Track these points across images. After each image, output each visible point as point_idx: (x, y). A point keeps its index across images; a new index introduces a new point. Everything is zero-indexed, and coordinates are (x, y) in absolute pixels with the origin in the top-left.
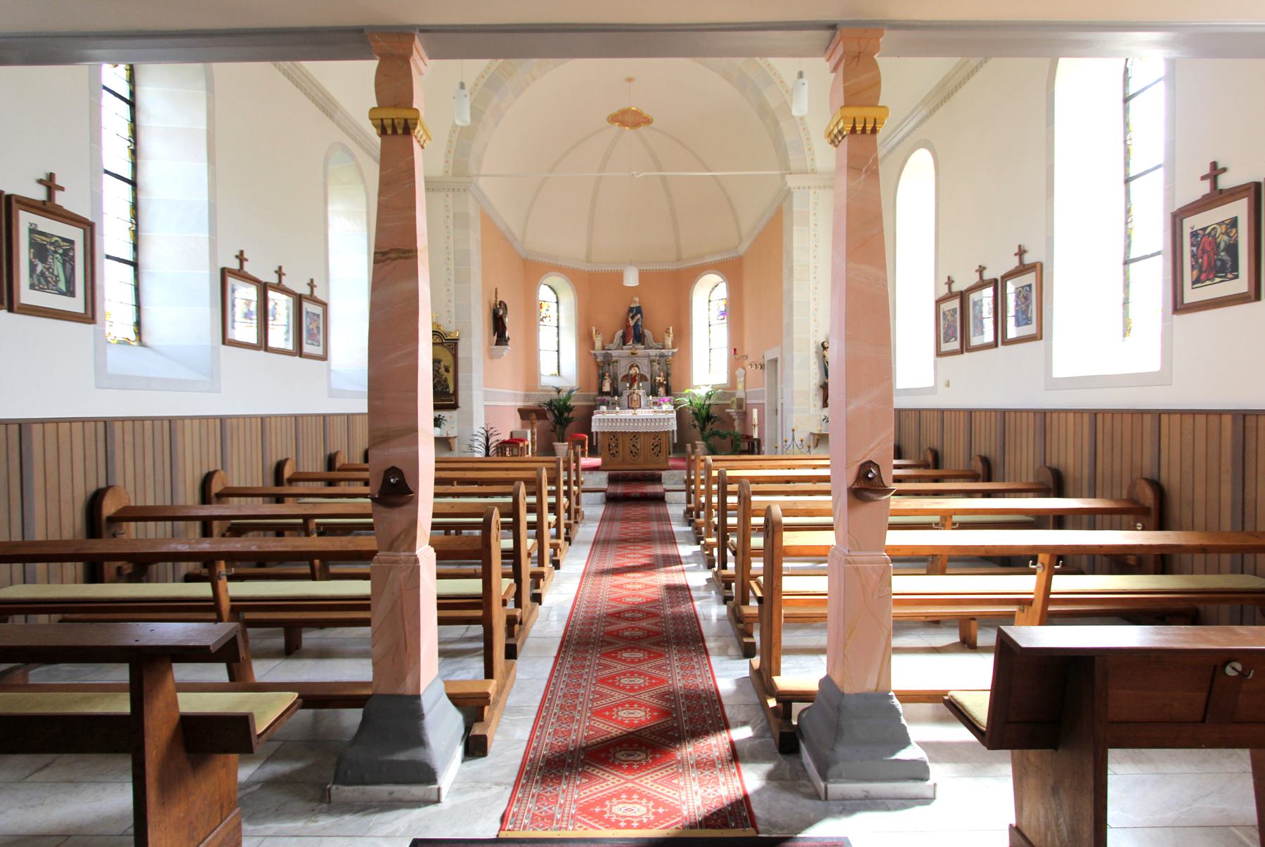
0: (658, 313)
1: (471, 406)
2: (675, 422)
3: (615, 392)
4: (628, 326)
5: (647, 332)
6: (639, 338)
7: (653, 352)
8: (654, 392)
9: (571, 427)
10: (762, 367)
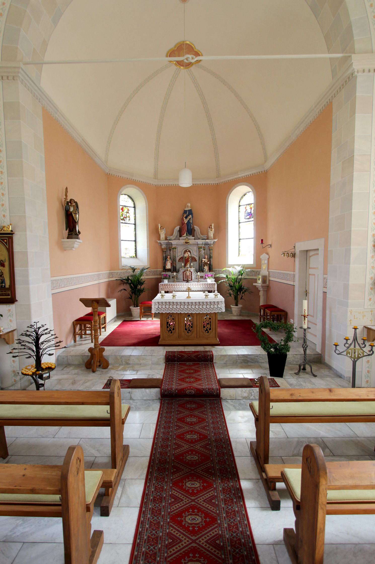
0: (204, 214)
1: (29, 300)
2: (223, 305)
3: (174, 269)
4: (183, 224)
5: (196, 228)
6: (191, 232)
7: (200, 242)
8: (201, 270)
10: (294, 255)
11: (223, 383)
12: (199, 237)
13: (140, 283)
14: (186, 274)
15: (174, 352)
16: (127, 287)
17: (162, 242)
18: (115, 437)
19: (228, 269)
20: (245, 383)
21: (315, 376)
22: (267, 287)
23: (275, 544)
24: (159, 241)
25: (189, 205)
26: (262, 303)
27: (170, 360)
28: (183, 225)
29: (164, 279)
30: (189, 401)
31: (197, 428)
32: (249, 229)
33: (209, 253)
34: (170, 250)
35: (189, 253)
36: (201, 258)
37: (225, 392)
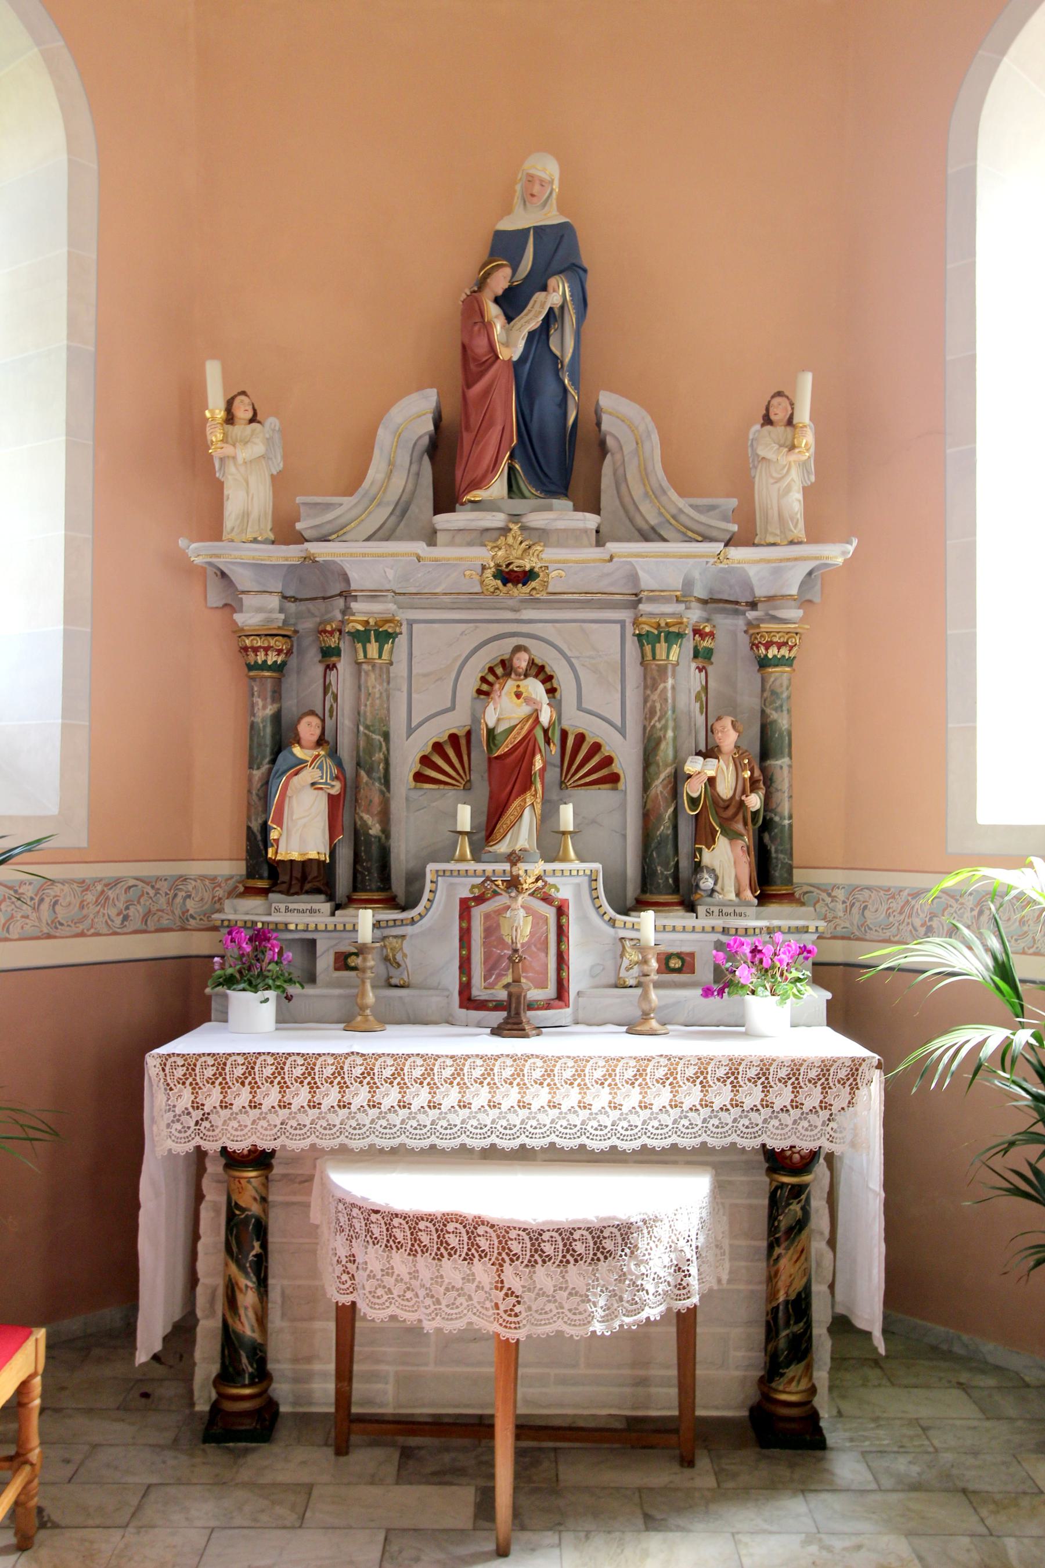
3: (368, 871)
5: (620, 415)
6: (558, 459)
7: (668, 567)
8: (662, 880)
12: (650, 514)
14: (491, 931)
19: (1001, 876)
24: (198, 552)
25: (547, 168)
28: (469, 381)
29: (230, 981)
33: (749, 700)
34: (329, 655)
35: (535, 688)
36: (666, 751)
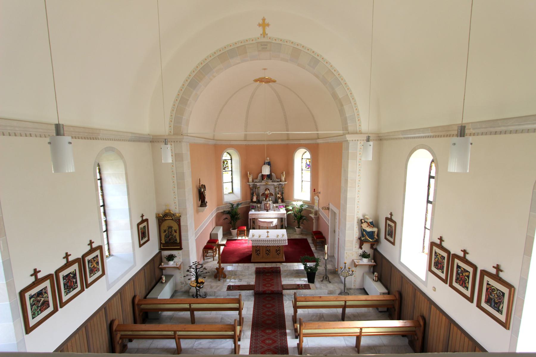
7: (276, 184)
8: (276, 202)
9: (238, 222)
11: (284, 287)
13: (236, 214)
15: (260, 268)
16: (228, 216)
17: (250, 184)
18: (240, 314)
20: (295, 287)
21: (330, 282)
22: (318, 218)
23: (294, 348)
26: (314, 230)
27: (259, 272)
30: (268, 295)
31: (271, 310)
32: (307, 175)
37: (285, 292)
